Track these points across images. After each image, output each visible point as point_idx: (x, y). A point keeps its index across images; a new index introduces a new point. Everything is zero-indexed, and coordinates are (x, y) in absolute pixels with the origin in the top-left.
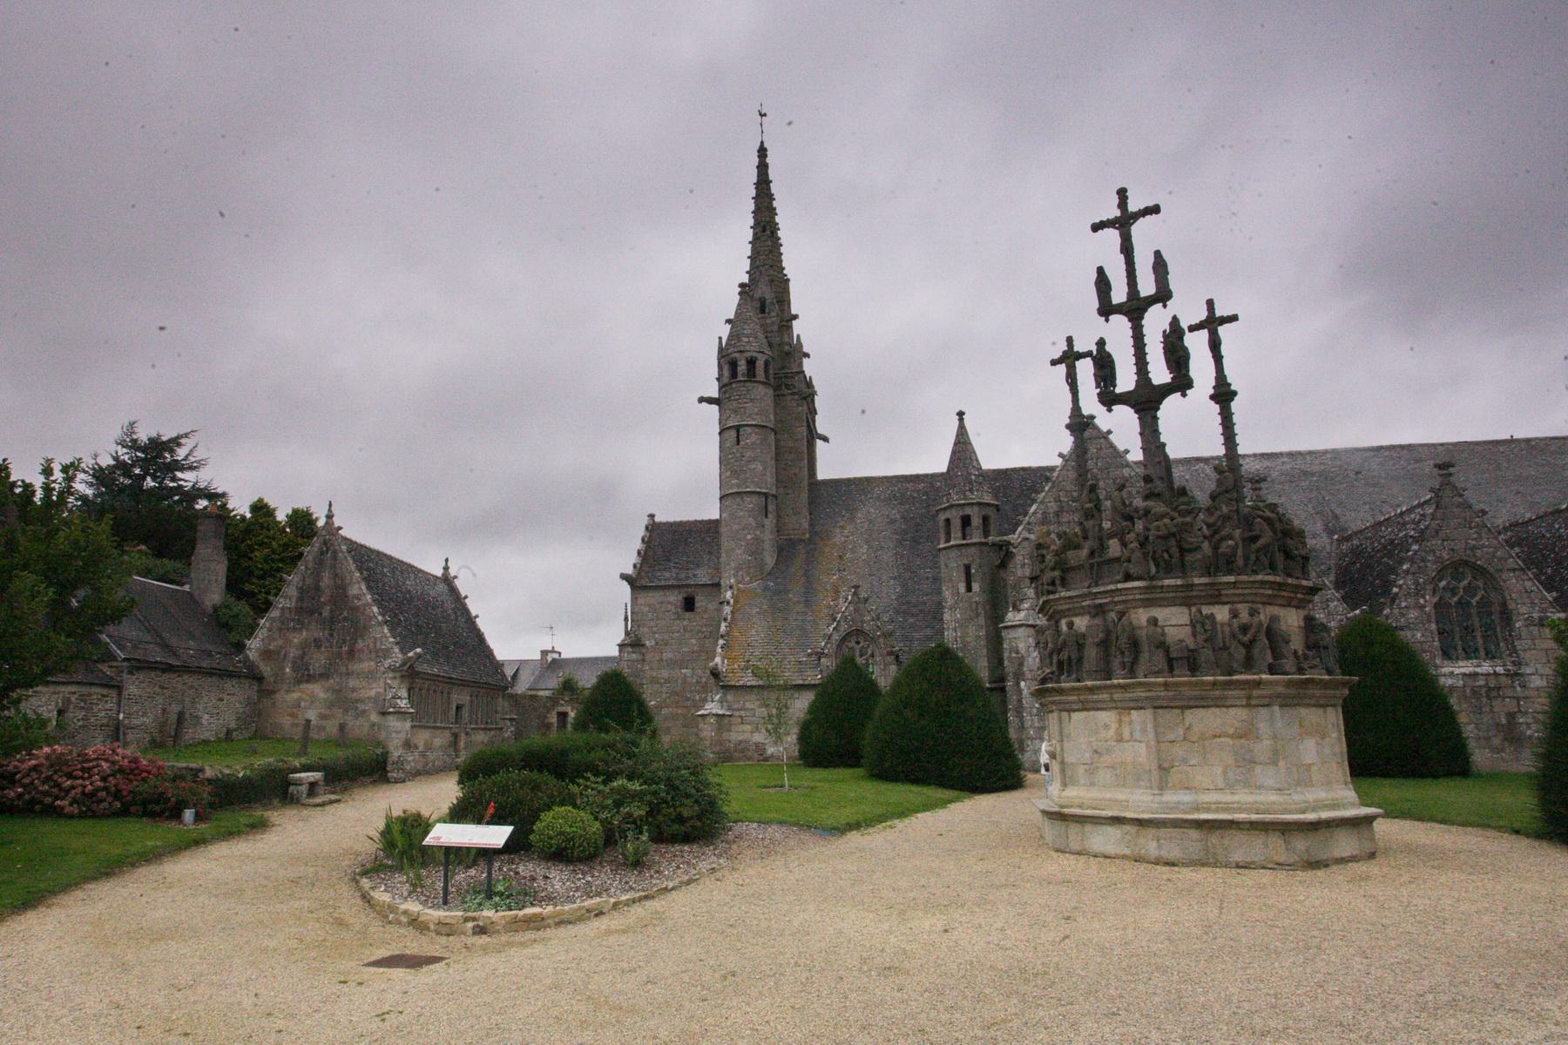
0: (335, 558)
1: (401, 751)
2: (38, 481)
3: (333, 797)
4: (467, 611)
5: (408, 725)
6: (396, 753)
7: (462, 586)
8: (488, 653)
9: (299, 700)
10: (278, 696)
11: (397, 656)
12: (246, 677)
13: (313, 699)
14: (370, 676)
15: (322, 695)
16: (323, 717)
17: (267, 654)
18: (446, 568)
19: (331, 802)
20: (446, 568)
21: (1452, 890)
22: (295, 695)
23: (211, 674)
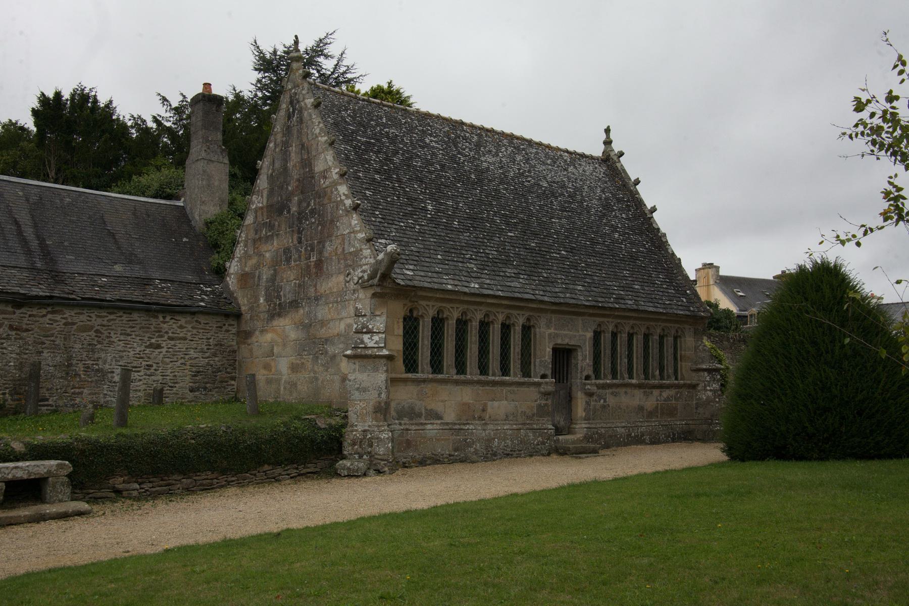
0: (301, 121)
1: (369, 423)
2: (162, 111)
3: (83, 506)
4: (640, 203)
5: (381, 377)
6: (361, 423)
7: (631, 167)
8: (671, 265)
9: (272, 344)
10: (254, 339)
11: (368, 259)
12: (205, 312)
13: (314, 344)
14: (340, 299)
15: (293, 335)
16: (294, 368)
17: (245, 278)
18: (608, 143)
19: (80, 514)
20: (608, 143)
21: (8, 104)
22: (269, 336)
23: (83, 306)
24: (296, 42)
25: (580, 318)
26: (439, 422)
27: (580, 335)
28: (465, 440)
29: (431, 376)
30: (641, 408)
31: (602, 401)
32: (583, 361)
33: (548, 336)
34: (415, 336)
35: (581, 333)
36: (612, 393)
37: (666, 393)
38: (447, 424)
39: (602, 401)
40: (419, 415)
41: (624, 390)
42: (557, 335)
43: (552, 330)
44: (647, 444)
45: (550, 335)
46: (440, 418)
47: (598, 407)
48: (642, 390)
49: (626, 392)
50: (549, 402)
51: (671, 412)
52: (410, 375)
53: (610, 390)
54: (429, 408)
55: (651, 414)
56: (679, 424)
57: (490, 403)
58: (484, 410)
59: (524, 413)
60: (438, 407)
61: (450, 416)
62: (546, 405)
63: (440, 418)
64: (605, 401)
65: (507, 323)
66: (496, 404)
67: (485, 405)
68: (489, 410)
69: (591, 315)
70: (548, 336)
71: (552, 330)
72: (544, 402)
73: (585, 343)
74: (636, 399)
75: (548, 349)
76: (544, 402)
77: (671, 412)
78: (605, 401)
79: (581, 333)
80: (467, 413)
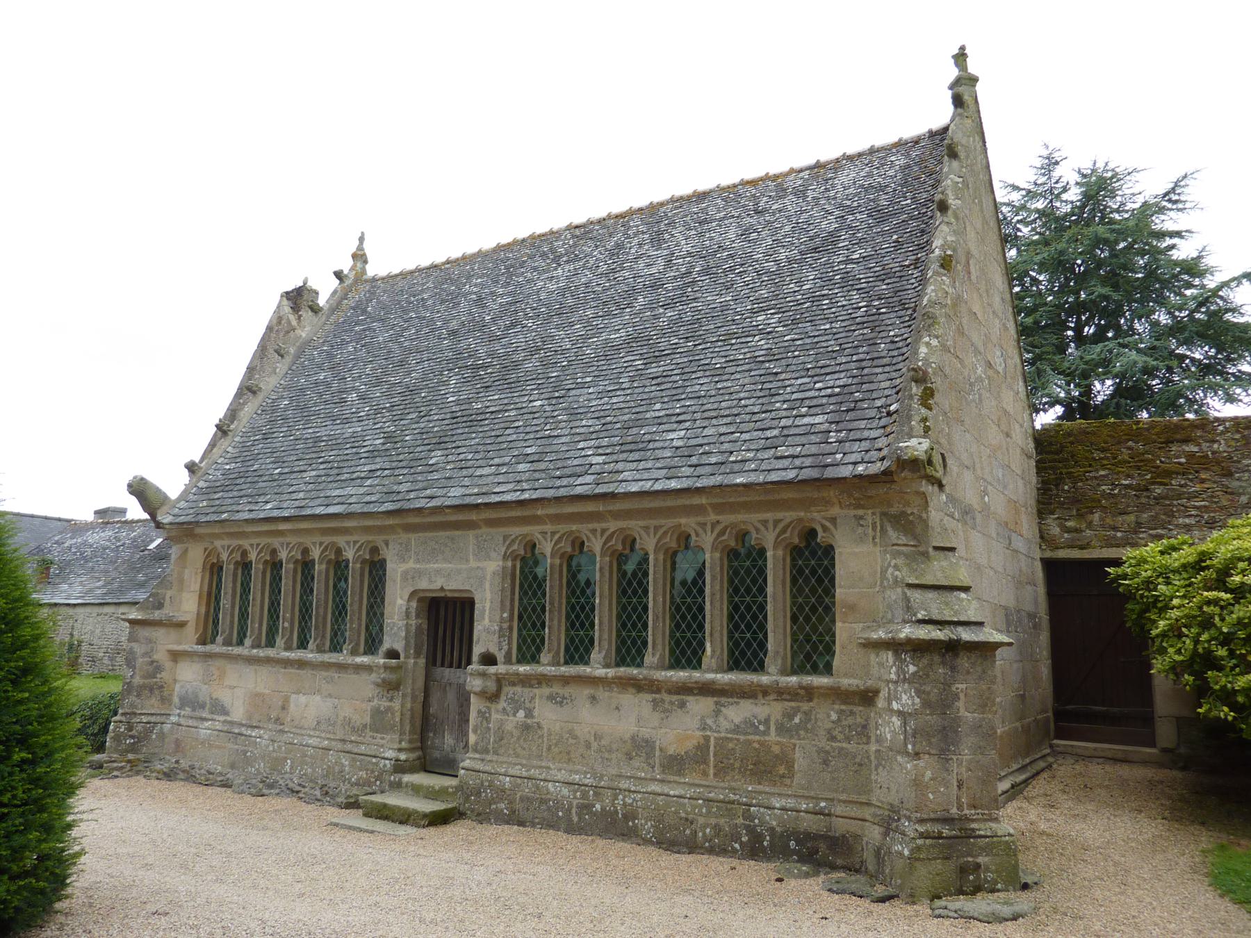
24: (360, 257)
25: (471, 534)
26: (222, 718)
27: (477, 572)
28: (245, 752)
29: (611, 672)
30: (641, 747)
31: (521, 714)
32: (489, 628)
33: (412, 573)
34: (624, 608)
35: (473, 564)
36: (551, 698)
37: (738, 712)
38: (232, 723)
39: (521, 714)
40: (203, 706)
41: (587, 691)
42: (420, 573)
43: (411, 564)
44: (647, 842)
45: (405, 573)
46: (226, 713)
47: (509, 727)
48: (649, 697)
49: (593, 698)
50: (396, 705)
51: (766, 767)
52: (682, 675)
53: (546, 691)
54: (214, 696)
55: (675, 764)
56: (778, 806)
57: (294, 696)
58: (283, 708)
59: (348, 722)
60: (224, 696)
61: (238, 714)
62: (389, 709)
63: (226, 713)
64: (529, 714)
65: (376, 559)
66: (303, 699)
67: (286, 700)
68: (292, 707)
69: (491, 523)
70: (412, 573)
71: (411, 564)
72: (385, 704)
73: (481, 584)
74: (629, 716)
75: (400, 602)
76: (385, 704)
77: (766, 767)
78: (529, 714)
79: (473, 564)
80: (271, 714)
